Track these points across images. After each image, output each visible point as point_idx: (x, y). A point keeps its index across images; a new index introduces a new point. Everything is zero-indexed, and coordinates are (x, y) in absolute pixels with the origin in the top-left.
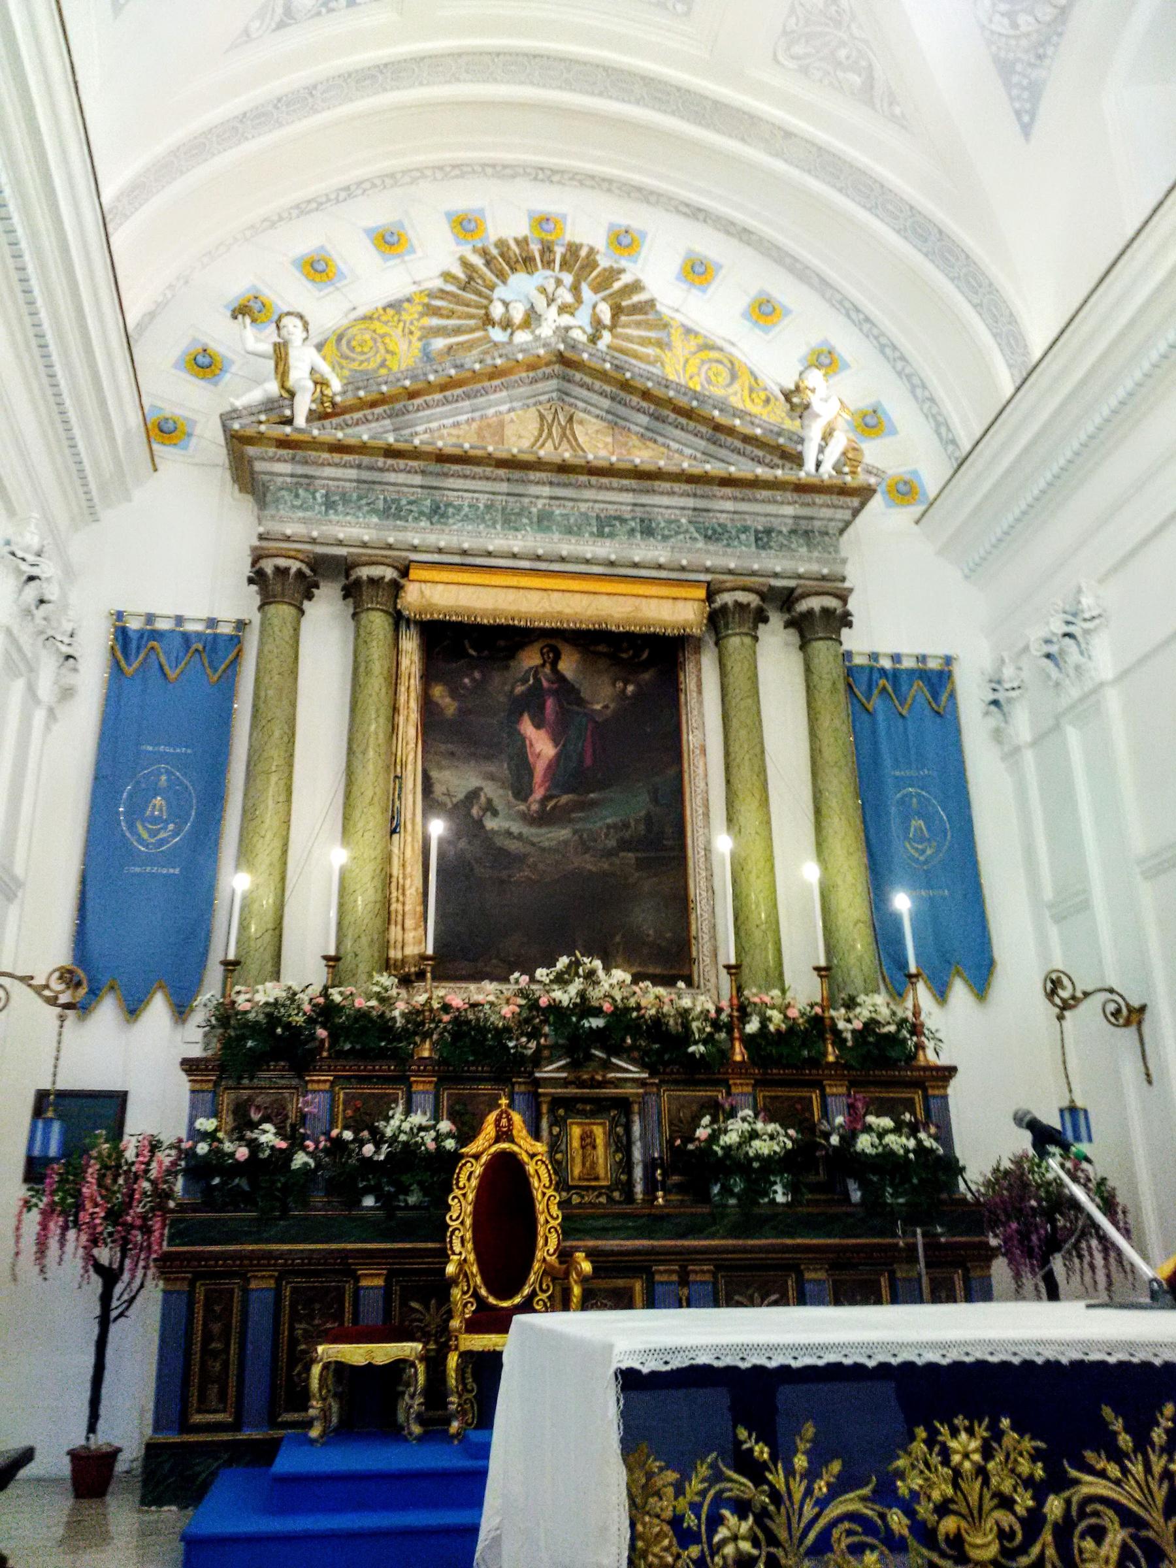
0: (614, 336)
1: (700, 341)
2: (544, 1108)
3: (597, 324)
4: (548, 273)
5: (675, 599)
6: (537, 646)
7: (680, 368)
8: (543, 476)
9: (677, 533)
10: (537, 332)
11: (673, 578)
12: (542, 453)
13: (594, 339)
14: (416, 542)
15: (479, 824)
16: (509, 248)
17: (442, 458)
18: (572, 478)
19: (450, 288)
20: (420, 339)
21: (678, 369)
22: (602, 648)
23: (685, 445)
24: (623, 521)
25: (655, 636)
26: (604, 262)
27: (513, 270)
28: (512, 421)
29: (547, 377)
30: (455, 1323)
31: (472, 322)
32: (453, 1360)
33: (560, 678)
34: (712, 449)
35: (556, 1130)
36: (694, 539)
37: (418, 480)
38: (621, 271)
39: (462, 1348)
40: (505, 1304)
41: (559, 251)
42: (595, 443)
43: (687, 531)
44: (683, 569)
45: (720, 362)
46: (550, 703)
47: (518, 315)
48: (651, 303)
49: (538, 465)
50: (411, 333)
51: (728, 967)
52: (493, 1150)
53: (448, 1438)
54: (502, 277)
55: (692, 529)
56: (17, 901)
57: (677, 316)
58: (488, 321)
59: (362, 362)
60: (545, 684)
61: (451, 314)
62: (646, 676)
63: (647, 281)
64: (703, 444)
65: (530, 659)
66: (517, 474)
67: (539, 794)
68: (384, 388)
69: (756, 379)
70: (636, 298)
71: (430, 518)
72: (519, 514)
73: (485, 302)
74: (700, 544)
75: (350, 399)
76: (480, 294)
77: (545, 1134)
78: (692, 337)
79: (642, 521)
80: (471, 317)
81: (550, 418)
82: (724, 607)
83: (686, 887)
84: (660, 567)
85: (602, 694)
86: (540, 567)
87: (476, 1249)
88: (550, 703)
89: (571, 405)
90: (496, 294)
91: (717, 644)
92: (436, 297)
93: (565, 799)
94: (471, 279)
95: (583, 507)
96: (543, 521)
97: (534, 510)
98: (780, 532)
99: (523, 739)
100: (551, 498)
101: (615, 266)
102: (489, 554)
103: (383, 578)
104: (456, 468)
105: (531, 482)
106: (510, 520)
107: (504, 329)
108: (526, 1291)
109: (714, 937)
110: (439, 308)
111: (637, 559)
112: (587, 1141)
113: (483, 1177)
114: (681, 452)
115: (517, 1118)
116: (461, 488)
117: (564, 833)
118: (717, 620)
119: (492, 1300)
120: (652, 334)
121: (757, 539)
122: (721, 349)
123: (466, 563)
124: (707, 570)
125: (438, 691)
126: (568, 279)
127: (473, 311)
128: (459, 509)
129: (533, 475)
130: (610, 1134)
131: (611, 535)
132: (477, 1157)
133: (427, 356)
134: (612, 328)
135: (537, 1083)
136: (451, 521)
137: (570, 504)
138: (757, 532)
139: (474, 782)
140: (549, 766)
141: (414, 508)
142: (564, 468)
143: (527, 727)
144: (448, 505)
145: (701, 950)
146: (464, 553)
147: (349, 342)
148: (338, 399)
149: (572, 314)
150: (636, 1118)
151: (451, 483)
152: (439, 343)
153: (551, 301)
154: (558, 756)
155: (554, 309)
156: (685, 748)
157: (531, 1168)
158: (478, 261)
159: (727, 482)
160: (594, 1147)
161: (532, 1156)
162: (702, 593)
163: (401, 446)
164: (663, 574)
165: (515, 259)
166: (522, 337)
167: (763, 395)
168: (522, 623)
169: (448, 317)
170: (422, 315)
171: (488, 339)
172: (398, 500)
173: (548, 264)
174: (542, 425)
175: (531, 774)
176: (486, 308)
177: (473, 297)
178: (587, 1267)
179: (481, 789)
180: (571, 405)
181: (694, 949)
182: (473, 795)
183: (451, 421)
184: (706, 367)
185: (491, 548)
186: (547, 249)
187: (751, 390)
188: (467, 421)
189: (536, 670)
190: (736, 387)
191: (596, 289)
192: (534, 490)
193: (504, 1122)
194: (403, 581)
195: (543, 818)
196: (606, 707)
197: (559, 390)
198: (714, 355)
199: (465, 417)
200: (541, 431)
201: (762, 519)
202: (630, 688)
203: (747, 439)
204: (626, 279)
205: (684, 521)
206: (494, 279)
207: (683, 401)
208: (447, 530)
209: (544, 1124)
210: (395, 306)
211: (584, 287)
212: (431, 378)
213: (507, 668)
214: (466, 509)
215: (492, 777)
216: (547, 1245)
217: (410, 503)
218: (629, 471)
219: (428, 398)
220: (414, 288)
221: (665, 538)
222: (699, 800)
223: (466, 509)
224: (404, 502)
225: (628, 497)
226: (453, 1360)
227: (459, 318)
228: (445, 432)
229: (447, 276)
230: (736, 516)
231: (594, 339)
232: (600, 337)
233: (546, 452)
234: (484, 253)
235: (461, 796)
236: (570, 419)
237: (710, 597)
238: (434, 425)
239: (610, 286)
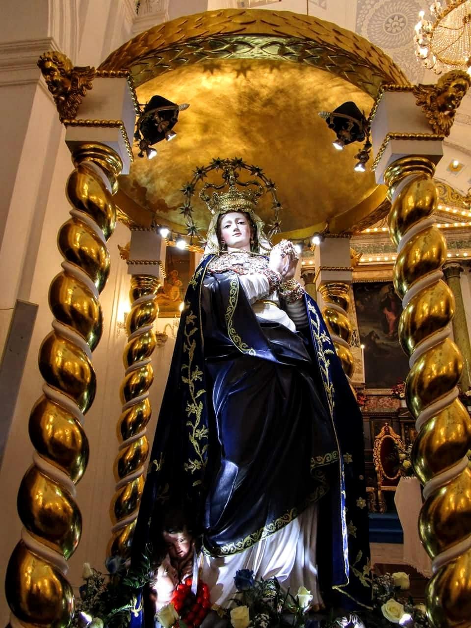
2: (402, 426)
6: (387, 286)
15: (374, 342)
30: (379, 483)
32: (379, 493)
34: (440, 218)
35: (406, 432)
40: (395, 478)
53: (380, 513)
69: (453, 190)
82: (448, 269)
87: (382, 464)
98: (465, 242)
108: (398, 475)
113: (382, 445)
115: (391, 428)
119: (388, 477)
121: (457, 245)
122: (440, 182)
125: (358, 303)
132: (380, 439)
138: (457, 243)
139: (371, 330)
143: (386, 311)
161: (396, 439)
187: (452, 194)
189: (387, 294)
190: (447, 194)
193: (387, 429)
209: (403, 430)
213: (378, 294)
214: (362, 249)
215: (377, 328)
226: (379, 493)
235: (368, 334)
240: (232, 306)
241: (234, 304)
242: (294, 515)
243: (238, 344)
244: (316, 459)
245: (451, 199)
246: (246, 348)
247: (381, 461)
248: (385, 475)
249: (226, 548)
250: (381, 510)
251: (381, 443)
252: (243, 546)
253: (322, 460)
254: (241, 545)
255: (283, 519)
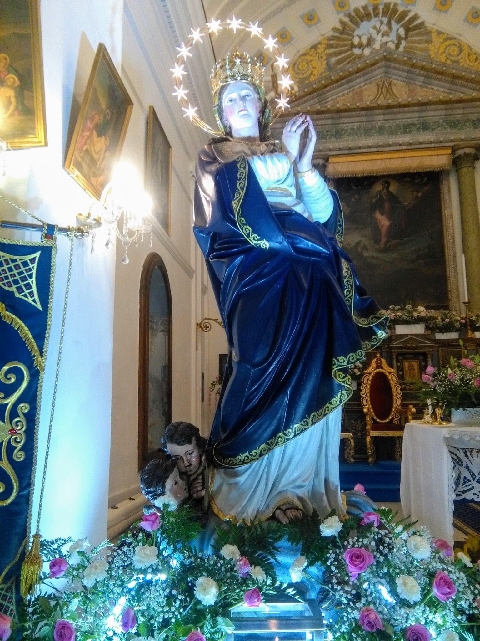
0: (407, 42)
1: (445, 36)
2: (394, 357)
3: (399, 38)
4: (377, 19)
5: (438, 155)
6: (381, 181)
7: (436, 51)
8: (380, 111)
9: (438, 127)
10: (373, 47)
11: (438, 146)
12: (379, 102)
13: (397, 47)
14: (331, 147)
16: (359, 11)
17: (339, 111)
18: (392, 110)
19: (337, 34)
20: (325, 60)
21: (437, 52)
22: (407, 179)
23: (440, 87)
24: (414, 124)
25: (430, 172)
26: (401, 9)
27: (362, 21)
28: (366, 89)
29: (381, 67)
30: (368, 427)
31: (346, 48)
32: (368, 439)
33: (390, 194)
35: (399, 364)
36: (445, 128)
37: (330, 121)
38: (409, 11)
39: (371, 435)
40: (387, 420)
41: (381, 7)
42: (401, 92)
43: (442, 125)
44: (441, 142)
45: (455, 45)
46: (387, 205)
47: (364, 40)
48: (422, 23)
49: (378, 107)
50: (322, 57)
51: (465, 303)
52: (376, 371)
54: (357, 25)
55: (445, 124)
56: (206, 294)
57: (434, 27)
58: (353, 46)
59: (303, 74)
60: (384, 197)
61: (338, 46)
62: (426, 189)
63: (420, 14)
64: (448, 85)
65: (378, 187)
66: (369, 112)
67: (384, 240)
68: (314, 86)
69: (471, 49)
70: (416, 23)
71: (335, 136)
72: (371, 129)
73: (351, 38)
74: (449, 130)
75: (302, 93)
76: (348, 34)
77: (395, 366)
78: (441, 35)
79: (423, 124)
80: (346, 45)
81: (381, 85)
82: (460, 156)
83: (445, 272)
84: (431, 142)
85: (408, 197)
86: (380, 149)
88: (387, 205)
89: (390, 78)
90: (356, 33)
91: (457, 171)
92: (331, 40)
93: (394, 241)
94: (344, 28)
95: (398, 122)
96: (381, 130)
97: (377, 126)
99: (376, 219)
100: (384, 120)
101: (406, 9)
102: (360, 148)
103: (319, 164)
104: (344, 114)
105: (375, 115)
106: (367, 132)
107: (360, 48)
109: (458, 290)
110: (332, 44)
111: (421, 141)
112: (411, 368)
113: (373, 381)
114: (439, 91)
116: (349, 122)
117: (395, 255)
118: (457, 162)
119: (378, 420)
120: (424, 38)
121: (474, 124)
122: (455, 39)
123: (351, 152)
124: (452, 141)
126: (385, 20)
127: (346, 42)
128: (347, 130)
129: (376, 112)
130: (420, 365)
131: (410, 132)
132: (370, 373)
133: (329, 67)
134: (406, 38)
135: (391, 348)
136: (344, 136)
137: (392, 121)
140: (388, 229)
141: (329, 133)
142: (389, 107)
143: (378, 215)
144: (342, 130)
145: (452, 295)
146: (350, 149)
147: (298, 66)
148: (297, 94)
149: (388, 36)
150: (430, 359)
151: (342, 120)
152: (333, 60)
153: (378, 32)
154: (391, 225)
155: (380, 35)
156: (444, 217)
157: (390, 377)
158: (347, 20)
159: (460, 101)
160: (414, 370)
161: (390, 373)
162: (450, 151)
163: (323, 109)
164: (433, 145)
165: (363, 15)
166: (367, 51)
167: (475, 57)
168: (374, 174)
169: (336, 47)
170: (325, 49)
171: (353, 54)
172: (323, 131)
173: (376, 15)
174: (378, 89)
175: (380, 234)
176: (352, 40)
177: (347, 37)
178: (414, 410)
179: (361, 241)
180: (390, 78)
181: (450, 295)
182: (358, 244)
183: (341, 94)
184: (448, 48)
185: (360, 145)
186: (376, 8)
187: (469, 55)
188: (348, 93)
189: (380, 192)
191: (398, 22)
192: (377, 118)
194: (326, 164)
195: (386, 250)
196: (410, 203)
197: (385, 72)
198: (452, 42)
199: (346, 91)
200: (378, 91)
201: (476, 115)
202: (420, 194)
203: (468, 80)
204: (411, 14)
205: (441, 121)
206: (354, 26)
207: (439, 68)
208: (343, 140)
209: (395, 361)
210: (315, 47)
211: (393, 22)
212: (333, 78)
214: (349, 131)
216: (397, 403)
217: (327, 132)
218: (418, 103)
219: (332, 86)
220: (322, 38)
221: (433, 130)
222: (450, 237)
223: (349, 131)
224: (325, 131)
225: (417, 114)
226: (368, 439)
227: (341, 47)
228: (339, 99)
229: (335, 29)
230: (463, 115)
231: (397, 47)
232: (401, 43)
233: (381, 101)
234: (349, 16)
236: (390, 84)
237: (453, 152)
238: (334, 97)
239: (404, 19)
240: (241, 191)
241: (242, 189)
242: (314, 421)
243: (248, 236)
244: (338, 361)
245: (468, 62)
246: (258, 240)
247: (371, 400)
248: (375, 418)
249: (240, 457)
250: (370, 460)
251: (371, 378)
252: (258, 455)
253: (344, 361)
254: (256, 453)
255: (302, 424)
